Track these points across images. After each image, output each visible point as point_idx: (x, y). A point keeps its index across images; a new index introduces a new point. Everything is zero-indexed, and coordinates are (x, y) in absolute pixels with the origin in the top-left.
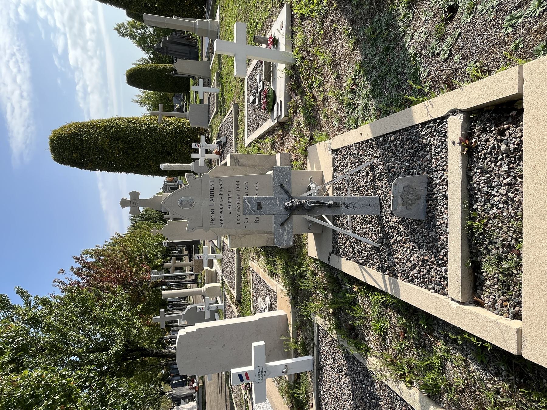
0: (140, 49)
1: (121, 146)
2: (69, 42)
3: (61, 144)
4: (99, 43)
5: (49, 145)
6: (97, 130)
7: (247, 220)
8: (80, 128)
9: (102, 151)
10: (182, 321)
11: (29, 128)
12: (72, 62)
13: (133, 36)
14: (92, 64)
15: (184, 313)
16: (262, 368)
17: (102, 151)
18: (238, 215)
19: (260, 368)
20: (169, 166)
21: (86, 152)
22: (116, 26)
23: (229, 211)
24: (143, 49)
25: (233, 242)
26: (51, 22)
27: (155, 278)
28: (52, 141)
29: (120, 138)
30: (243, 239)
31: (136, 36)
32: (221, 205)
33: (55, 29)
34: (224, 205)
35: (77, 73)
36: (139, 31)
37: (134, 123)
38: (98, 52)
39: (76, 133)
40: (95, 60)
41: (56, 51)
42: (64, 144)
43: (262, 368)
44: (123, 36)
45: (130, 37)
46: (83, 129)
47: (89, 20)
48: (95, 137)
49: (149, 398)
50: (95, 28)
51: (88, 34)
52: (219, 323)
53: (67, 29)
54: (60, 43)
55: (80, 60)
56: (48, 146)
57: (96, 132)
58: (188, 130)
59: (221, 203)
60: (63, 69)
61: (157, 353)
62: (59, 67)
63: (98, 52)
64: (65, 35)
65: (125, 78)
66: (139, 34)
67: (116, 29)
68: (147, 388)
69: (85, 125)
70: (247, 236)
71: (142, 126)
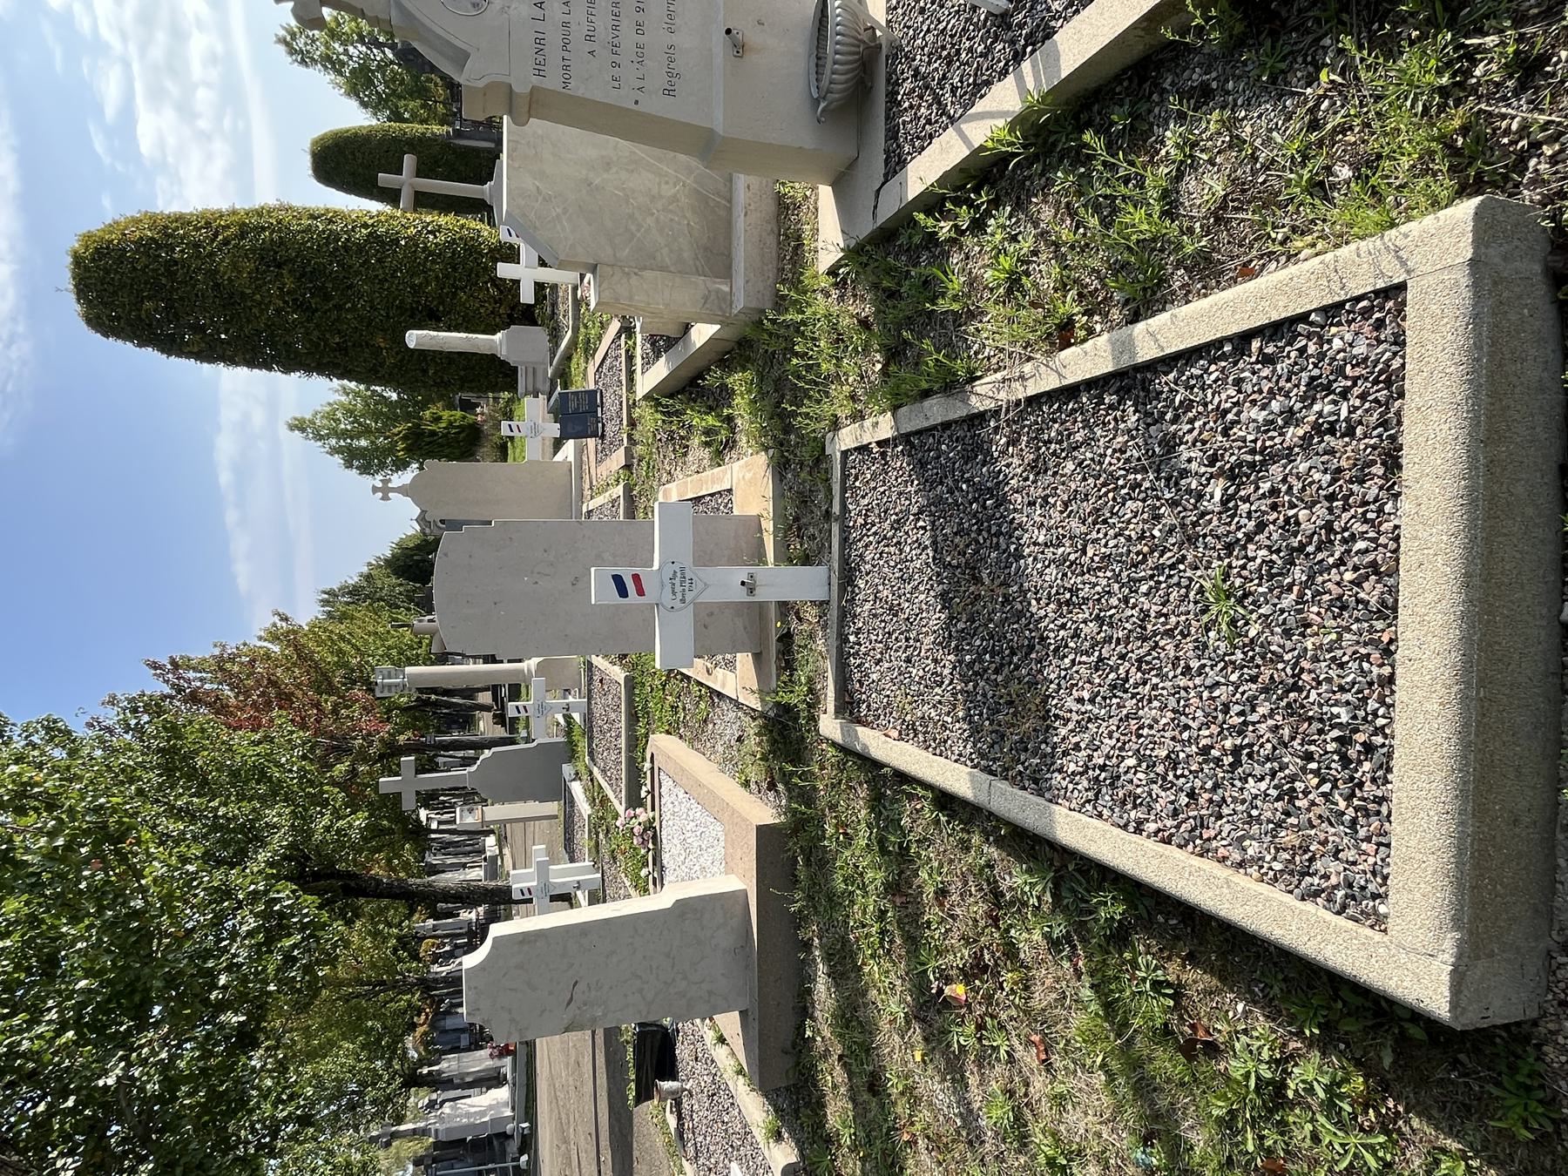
0: (353, 104)
1: (290, 284)
2: (138, 86)
3: (107, 272)
4: (231, 96)
5: (69, 275)
6: (216, 235)
7: (640, 84)
8: (166, 227)
9: (231, 296)
10: (466, 813)
11: (14, 348)
12: (146, 145)
13: (333, 63)
14: (209, 157)
15: (473, 768)
16: (682, 569)
17: (231, 296)
18: (615, 65)
19: (676, 567)
20: (433, 338)
21: (181, 299)
22: (282, 33)
23: (588, 46)
24: (364, 105)
25: (605, 285)
26: (84, 24)
27: (390, 686)
28: (78, 260)
29: (290, 260)
30: (634, 281)
31: (343, 64)
32: (565, 24)
33: (98, 47)
34: (573, 27)
35: (161, 182)
36: (351, 49)
37: (330, 221)
38: (227, 123)
39: (152, 239)
40: (218, 146)
41: (99, 110)
42: (116, 272)
43: (682, 569)
44: (303, 62)
45: (326, 67)
46: (177, 228)
47: (200, 25)
48: (212, 254)
49: (371, 1093)
50: (219, 48)
51: (197, 70)
52: (585, 913)
53: (133, 48)
54: (111, 91)
55: (171, 141)
56: (66, 280)
57: (213, 241)
58: (491, 250)
59: (566, 18)
60: (119, 168)
61: (390, 885)
62: (107, 160)
63: (227, 123)
64: (127, 65)
65: (307, 161)
66: (351, 57)
67: (284, 41)
68: (363, 1065)
69: (180, 219)
70: (648, 274)
71: (353, 229)
